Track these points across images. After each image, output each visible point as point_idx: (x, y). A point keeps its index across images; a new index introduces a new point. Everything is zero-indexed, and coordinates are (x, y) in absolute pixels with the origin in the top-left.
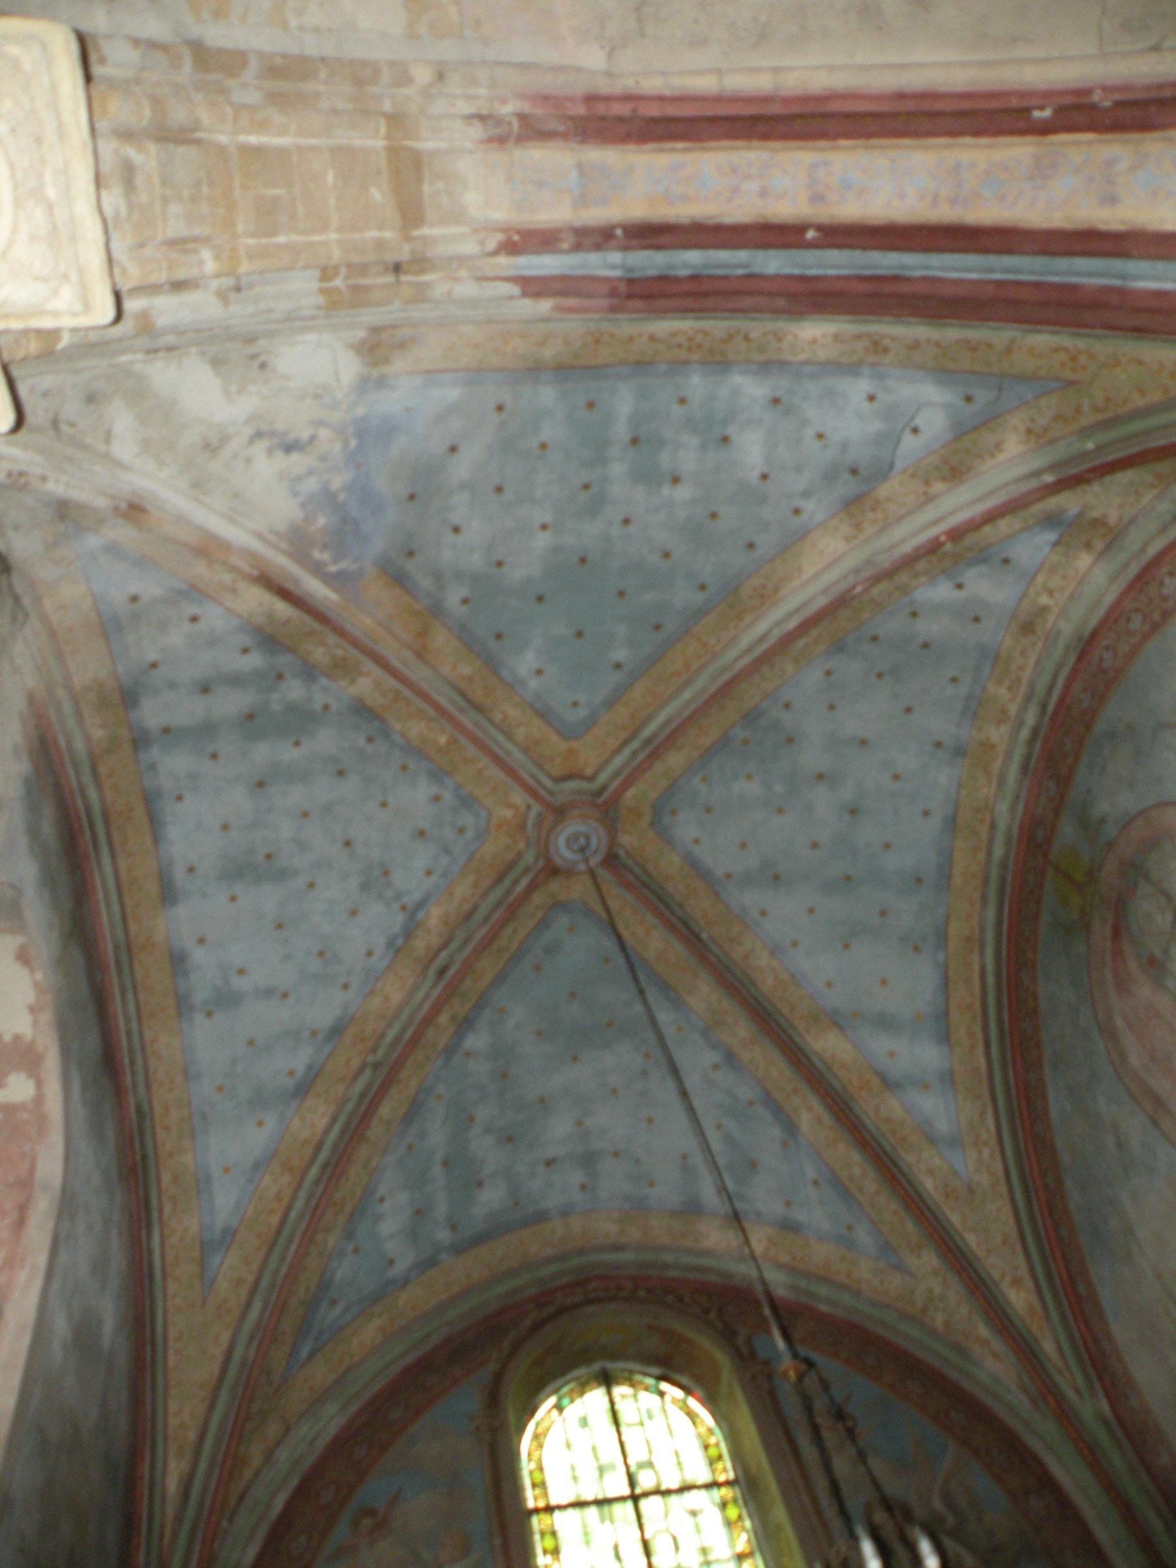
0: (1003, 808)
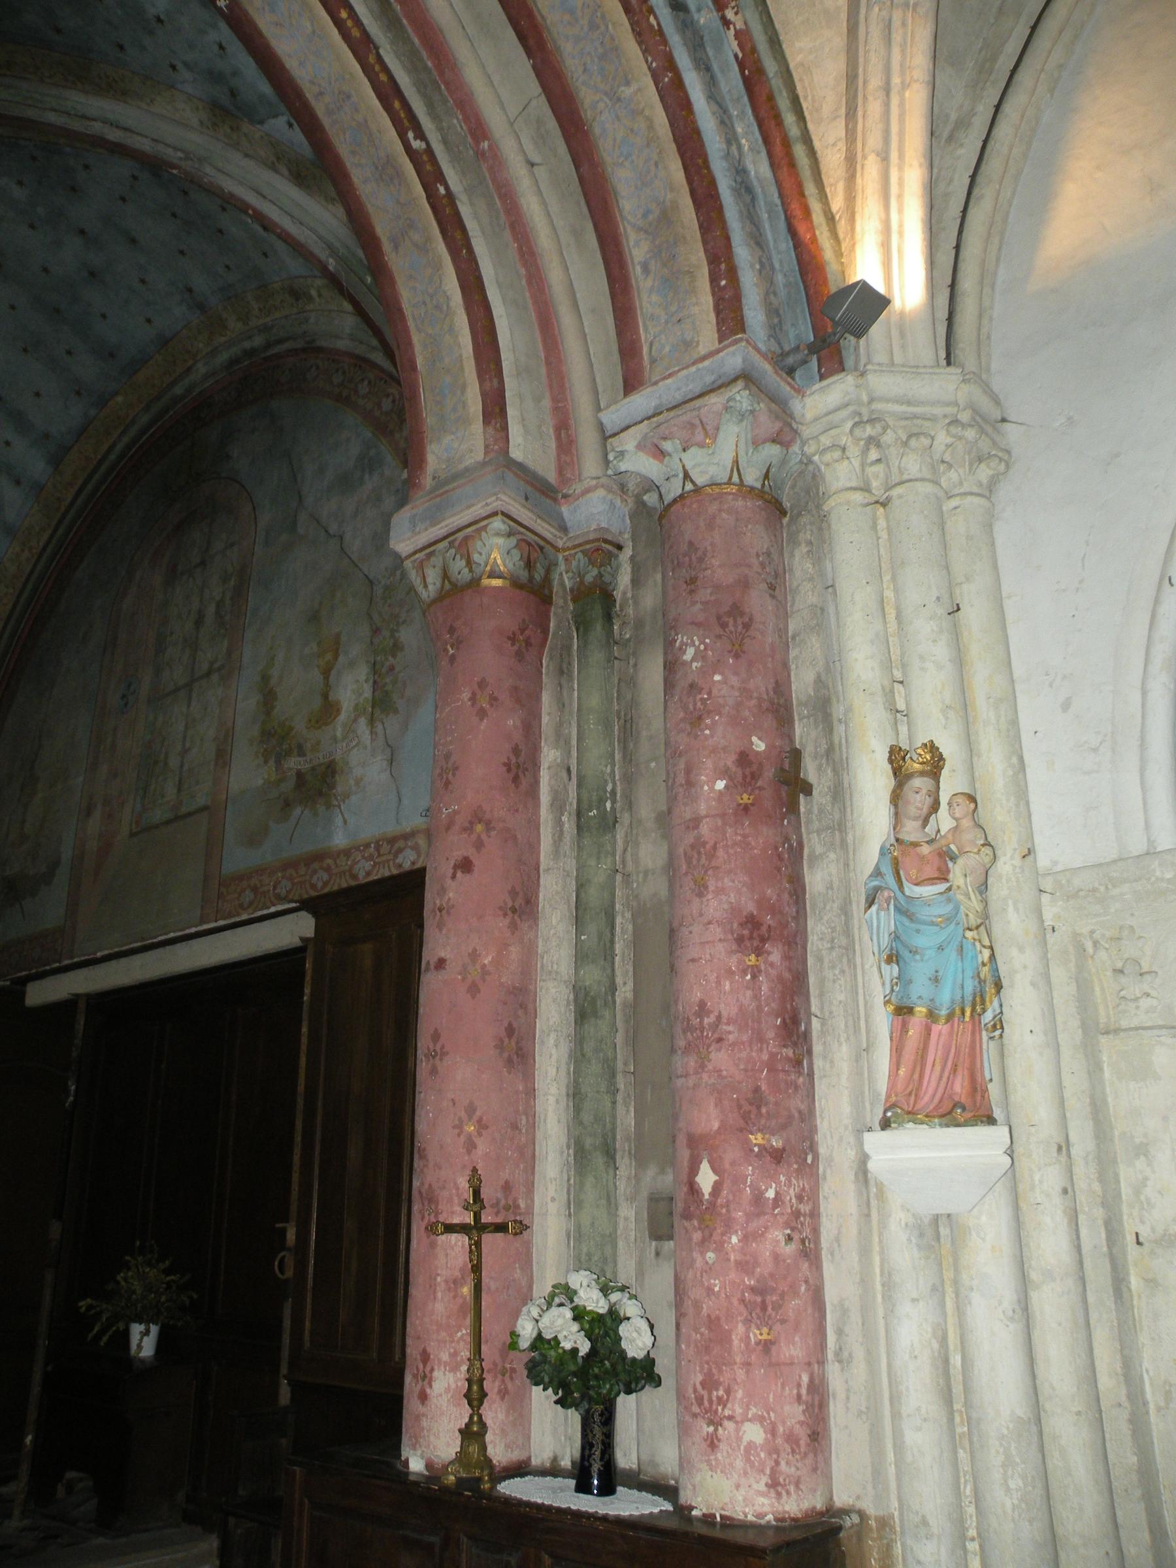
0: (201, 369)
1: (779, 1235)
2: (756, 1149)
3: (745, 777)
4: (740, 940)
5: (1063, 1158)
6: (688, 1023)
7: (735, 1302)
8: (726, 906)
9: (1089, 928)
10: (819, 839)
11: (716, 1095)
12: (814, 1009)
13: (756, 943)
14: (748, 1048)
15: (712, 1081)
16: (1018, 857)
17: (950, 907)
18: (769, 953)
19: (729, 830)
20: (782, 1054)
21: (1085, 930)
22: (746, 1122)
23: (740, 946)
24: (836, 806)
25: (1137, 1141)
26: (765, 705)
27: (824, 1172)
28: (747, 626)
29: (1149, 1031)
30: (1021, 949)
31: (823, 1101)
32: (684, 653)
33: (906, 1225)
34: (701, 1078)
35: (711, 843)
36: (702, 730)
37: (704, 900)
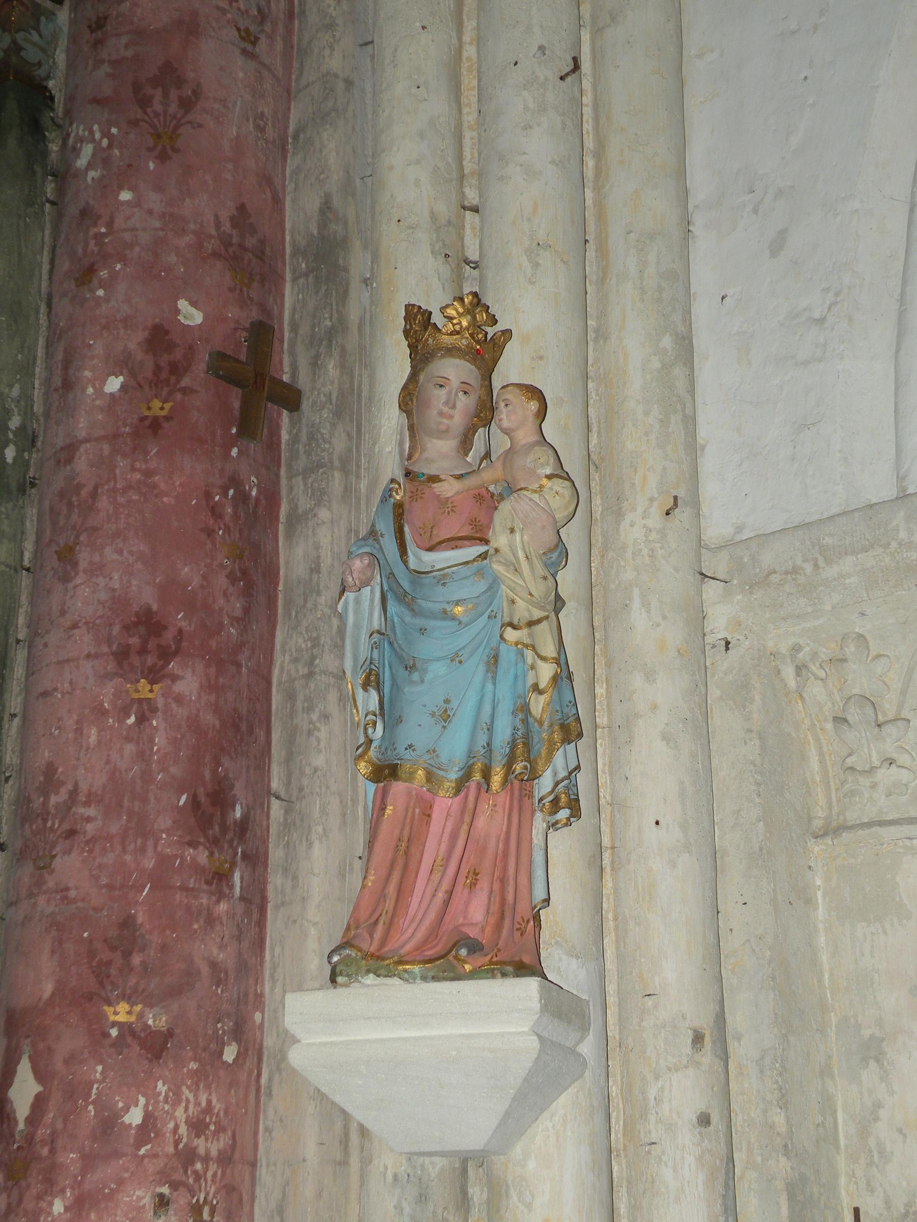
2: (114, 1032)
3: (158, 369)
4: (122, 655)
5: (707, 1057)
6: (28, 808)
8: (103, 596)
9: (791, 641)
10: (305, 485)
11: (54, 933)
12: (275, 785)
13: (150, 660)
14: (119, 847)
15: (51, 908)
16: (656, 512)
17: (482, 586)
18: (175, 678)
19: (122, 463)
20: (183, 860)
21: (784, 648)
25: (866, 1033)
26: (210, 246)
27: (270, 1080)
28: (187, 105)
29: (892, 829)
30: (649, 676)
31: (278, 950)
32: (78, 156)
33: (396, 1177)
34: (35, 905)
35: (90, 487)
36: (92, 291)
37: (70, 586)
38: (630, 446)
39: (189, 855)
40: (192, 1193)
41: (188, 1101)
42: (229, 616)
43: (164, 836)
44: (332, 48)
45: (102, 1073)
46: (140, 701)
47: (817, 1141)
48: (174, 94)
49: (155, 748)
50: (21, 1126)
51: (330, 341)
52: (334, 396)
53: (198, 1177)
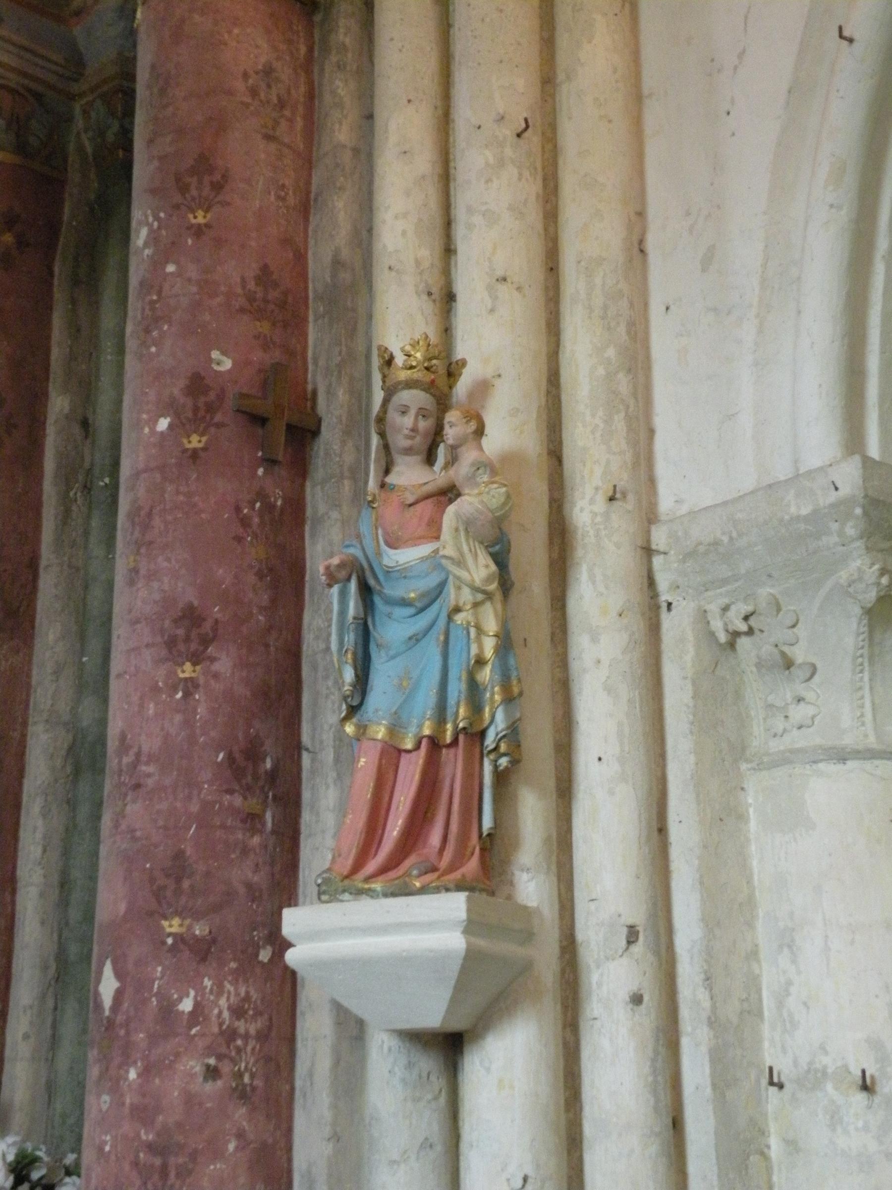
1: (194, 1065)
2: (170, 941)
3: (196, 410)
4: (171, 643)
7: (127, 1167)
13: (193, 646)
18: (213, 660)
19: (170, 488)
22: (159, 902)
23: (170, 652)
24: (350, 444)
26: (241, 301)
28: (217, 187)
30: (595, 640)
37: (135, 588)
38: (580, 443)
39: (227, 800)
40: (234, 1062)
41: (229, 993)
42: (257, 606)
43: (206, 786)
44: (341, 123)
45: (161, 972)
46: (186, 679)
47: (741, 1013)
48: (207, 179)
49: (198, 717)
50: (107, 1013)
51: (340, 372)
52: (344, 418)
53: (239, 1050)
